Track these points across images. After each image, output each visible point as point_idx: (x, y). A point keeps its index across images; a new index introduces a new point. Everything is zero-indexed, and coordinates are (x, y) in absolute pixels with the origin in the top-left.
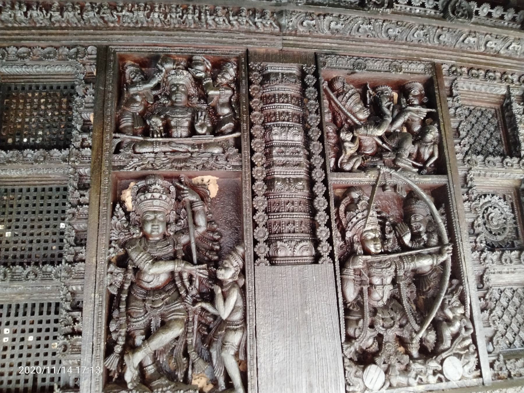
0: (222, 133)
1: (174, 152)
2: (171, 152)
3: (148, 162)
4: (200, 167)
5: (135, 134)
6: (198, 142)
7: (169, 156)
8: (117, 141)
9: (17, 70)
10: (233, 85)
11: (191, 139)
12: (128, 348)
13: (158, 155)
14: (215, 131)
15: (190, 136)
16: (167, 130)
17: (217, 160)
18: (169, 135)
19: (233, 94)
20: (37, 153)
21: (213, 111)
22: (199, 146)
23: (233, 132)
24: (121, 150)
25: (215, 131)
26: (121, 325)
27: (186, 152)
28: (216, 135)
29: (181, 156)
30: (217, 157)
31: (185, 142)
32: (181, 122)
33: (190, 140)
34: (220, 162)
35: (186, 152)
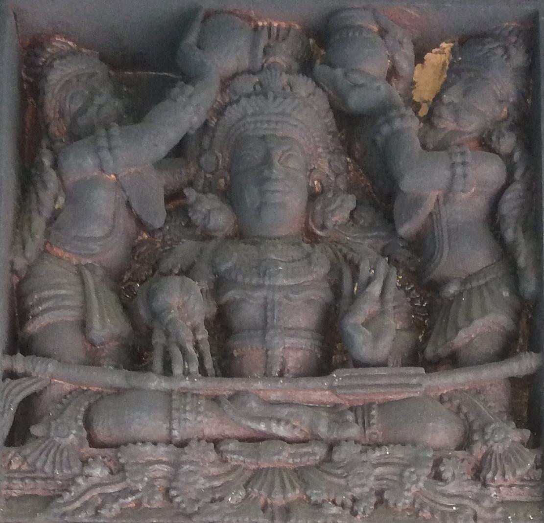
0: (453, 361)
1: (255, 439)
2: (242, 440)
3: (150, 485)
4: (367, 507)
5: (92, 360)
6: (359, 396)
7: (235, 459)
8: (20, 391)
9: (19, 398)
10: (507, 142)
11: (325, 382)
12: (103, 497)
13: (189, 454)
14: (426, 352)
15: (322, 367)
16: (225, 346)
17: (438, 476)
18: (226, 365)
19: (510, 180)
20: (386, 477)
21: (417, 262)
22: (362, 412)
23: (504, 353)
24: (36, 430)
25: (426, 352)
26: (104, 426)
27: (305, 442)
28: (432, 365)
29: (285, 457)
30: (438, 462)
31: (299, 396)
32: (287, 300)
33: (318, 391)
34: (451, 488)
35: (305, 442)
